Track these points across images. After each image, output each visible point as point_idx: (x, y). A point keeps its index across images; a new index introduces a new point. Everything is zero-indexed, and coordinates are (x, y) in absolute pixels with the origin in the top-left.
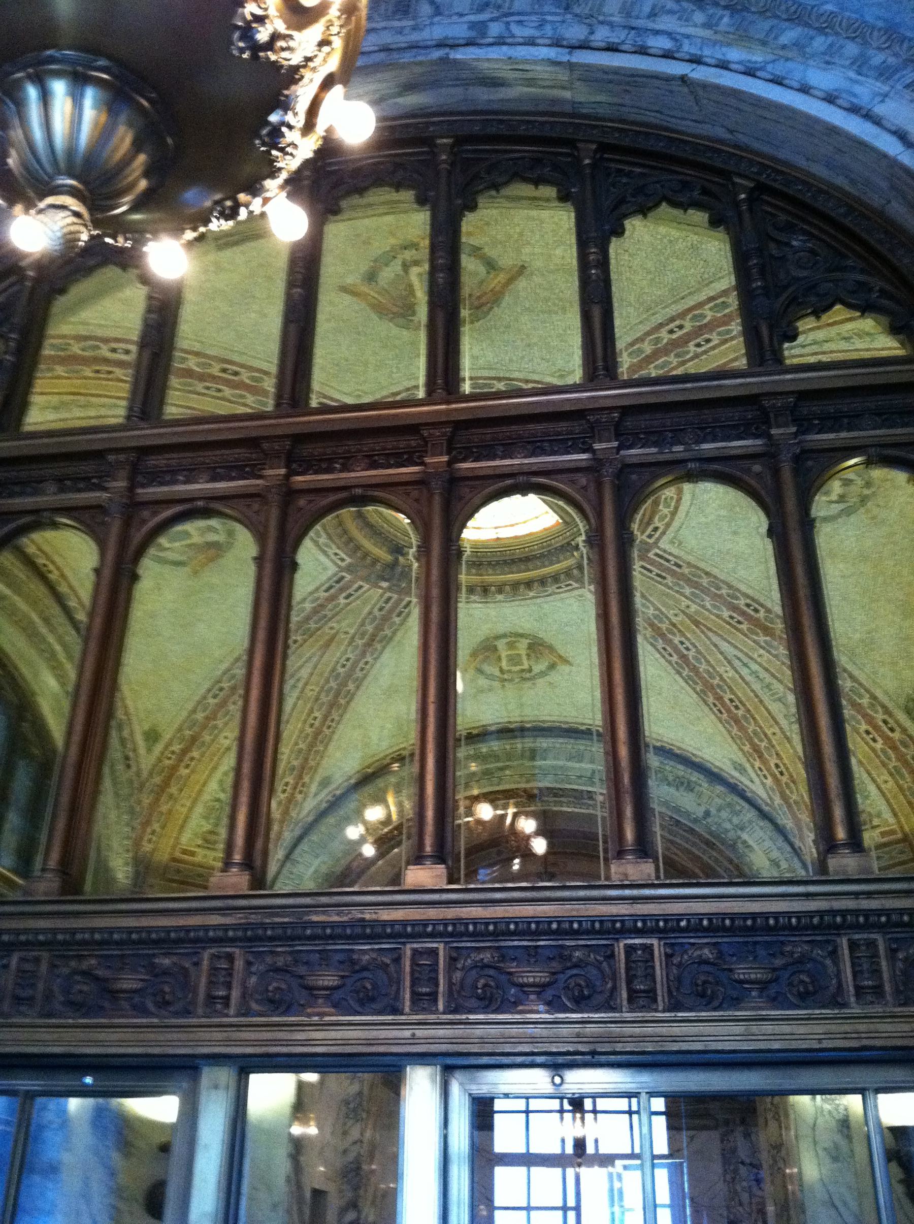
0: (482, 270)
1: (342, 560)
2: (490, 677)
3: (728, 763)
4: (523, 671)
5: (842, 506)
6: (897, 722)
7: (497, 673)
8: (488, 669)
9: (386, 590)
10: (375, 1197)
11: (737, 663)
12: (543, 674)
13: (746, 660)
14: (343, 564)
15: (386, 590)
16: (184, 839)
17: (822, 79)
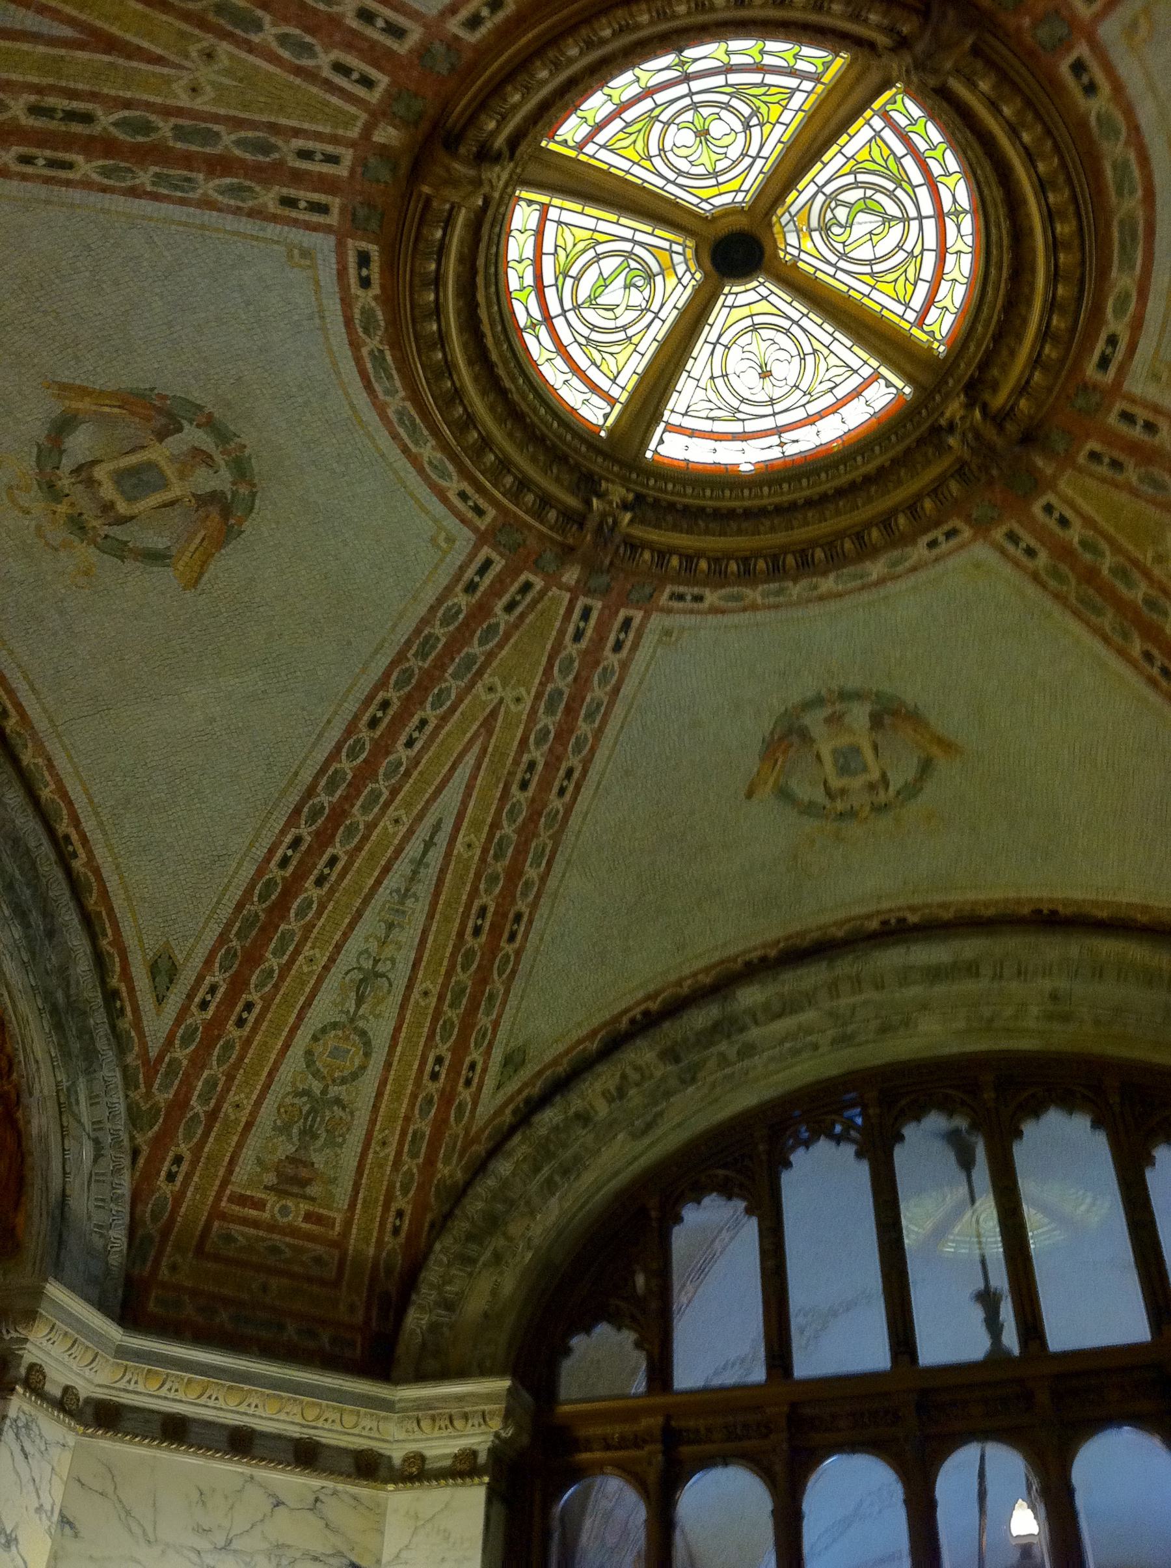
12: (911, 791)
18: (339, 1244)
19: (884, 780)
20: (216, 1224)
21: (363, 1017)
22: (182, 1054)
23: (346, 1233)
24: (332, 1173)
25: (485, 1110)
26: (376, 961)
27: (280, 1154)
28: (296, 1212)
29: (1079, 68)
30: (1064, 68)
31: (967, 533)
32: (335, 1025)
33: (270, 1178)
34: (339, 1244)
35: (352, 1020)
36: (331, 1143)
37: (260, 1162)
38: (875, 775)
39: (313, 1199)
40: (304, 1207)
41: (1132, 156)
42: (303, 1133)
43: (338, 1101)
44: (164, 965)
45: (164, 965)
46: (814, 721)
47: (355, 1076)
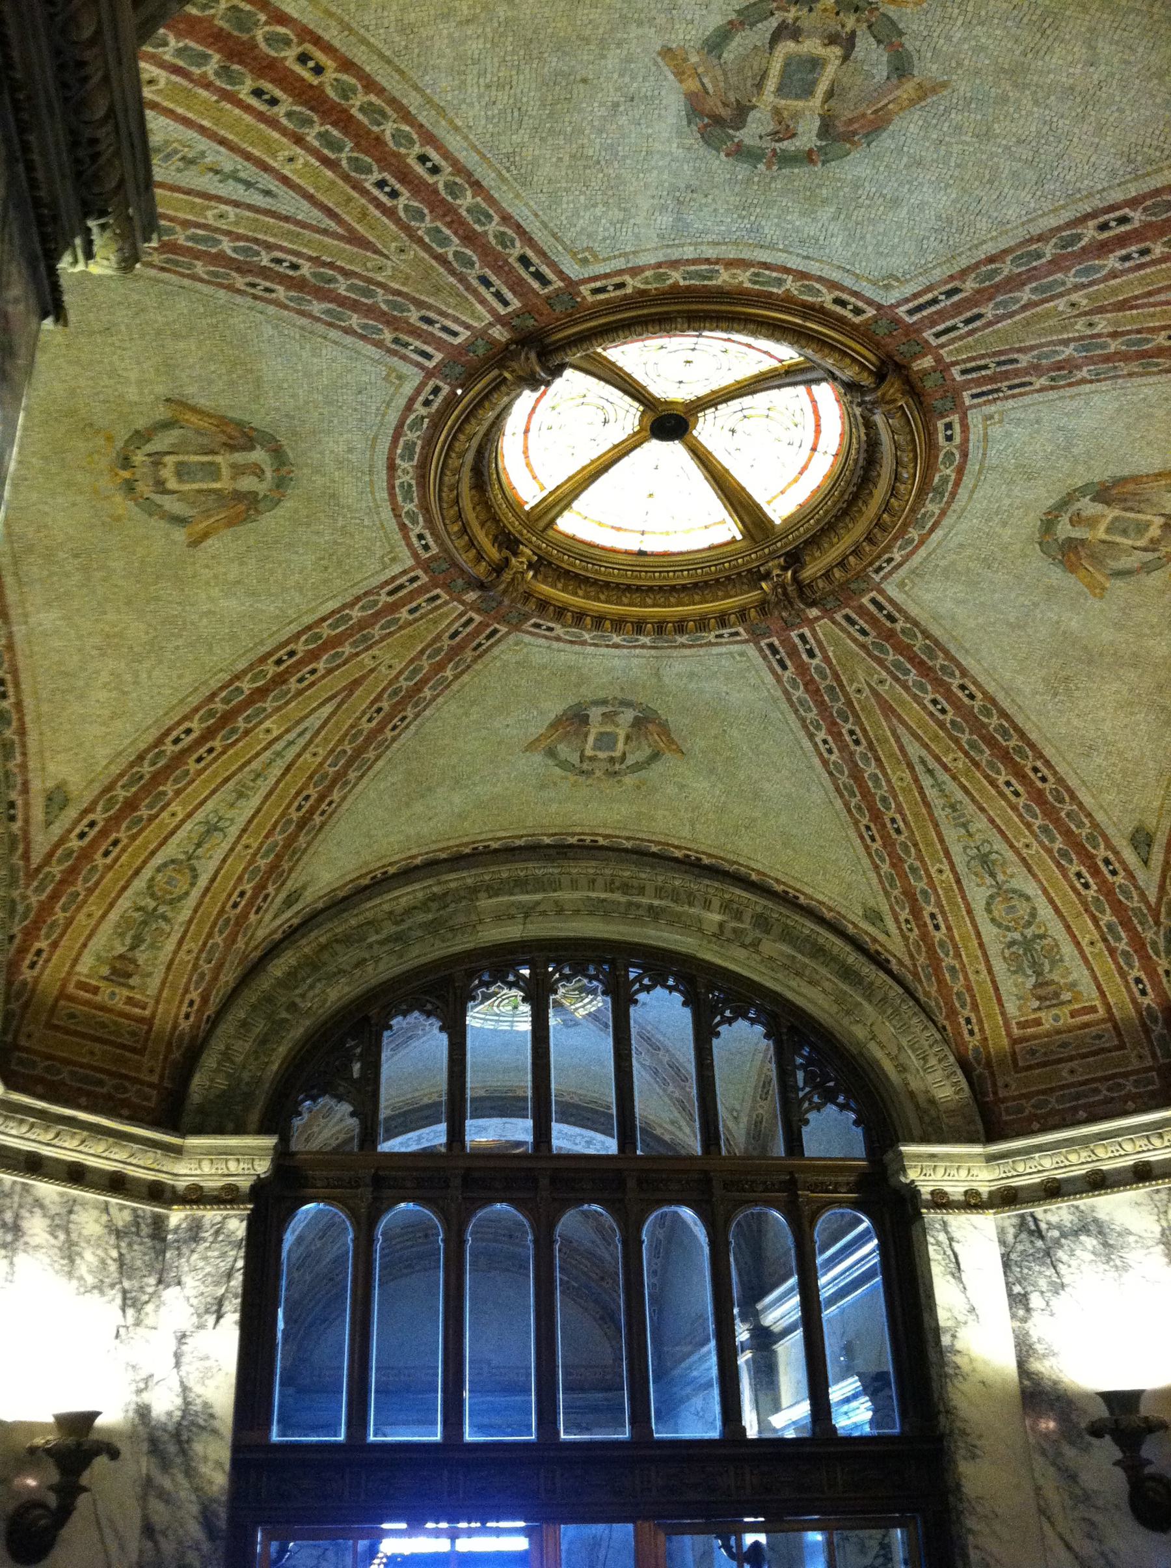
0: (881, 72)
1: (426, 547)
2: (564, 765)
3: (303, 879)
4: (612, 760)
5: (1150, 556)
6: (1122, 862)
7: (574, 758)
8: (563, 750)
9: (472, 606)
10: (881, 109)
11: (919, 768)
12: (637, 767)
13: (932, 764)
14: (430, 364)
15: (472, 606)
16: (83, 968)
17: (403, 900)
18: (149, 1021)
19: (623, 757)
20: (62, 1003)
21: (198, 858)
22: (56, 870)
23: (1108, 1008)
24: (150, 969)
25: (261, 933)
26: (220, 819)
27: (116, 953)
28: (115, 997)
29: (949, 426)
30: (940, 425)
31: (744, 636)
32: (991, 897)
33: (105, 971)
34: (149, 1021)
35: (189, 859)
36: (152, 946)
37: (99, 958)
38: (617, 754)
39: (133, 988)
40: (126, 993)
41: (953, 477)
42: (135, 937)
43: (164, 918)
44: (58, 798)
45: (58, 798)
46: (595, 713)
47: (180, 898)
